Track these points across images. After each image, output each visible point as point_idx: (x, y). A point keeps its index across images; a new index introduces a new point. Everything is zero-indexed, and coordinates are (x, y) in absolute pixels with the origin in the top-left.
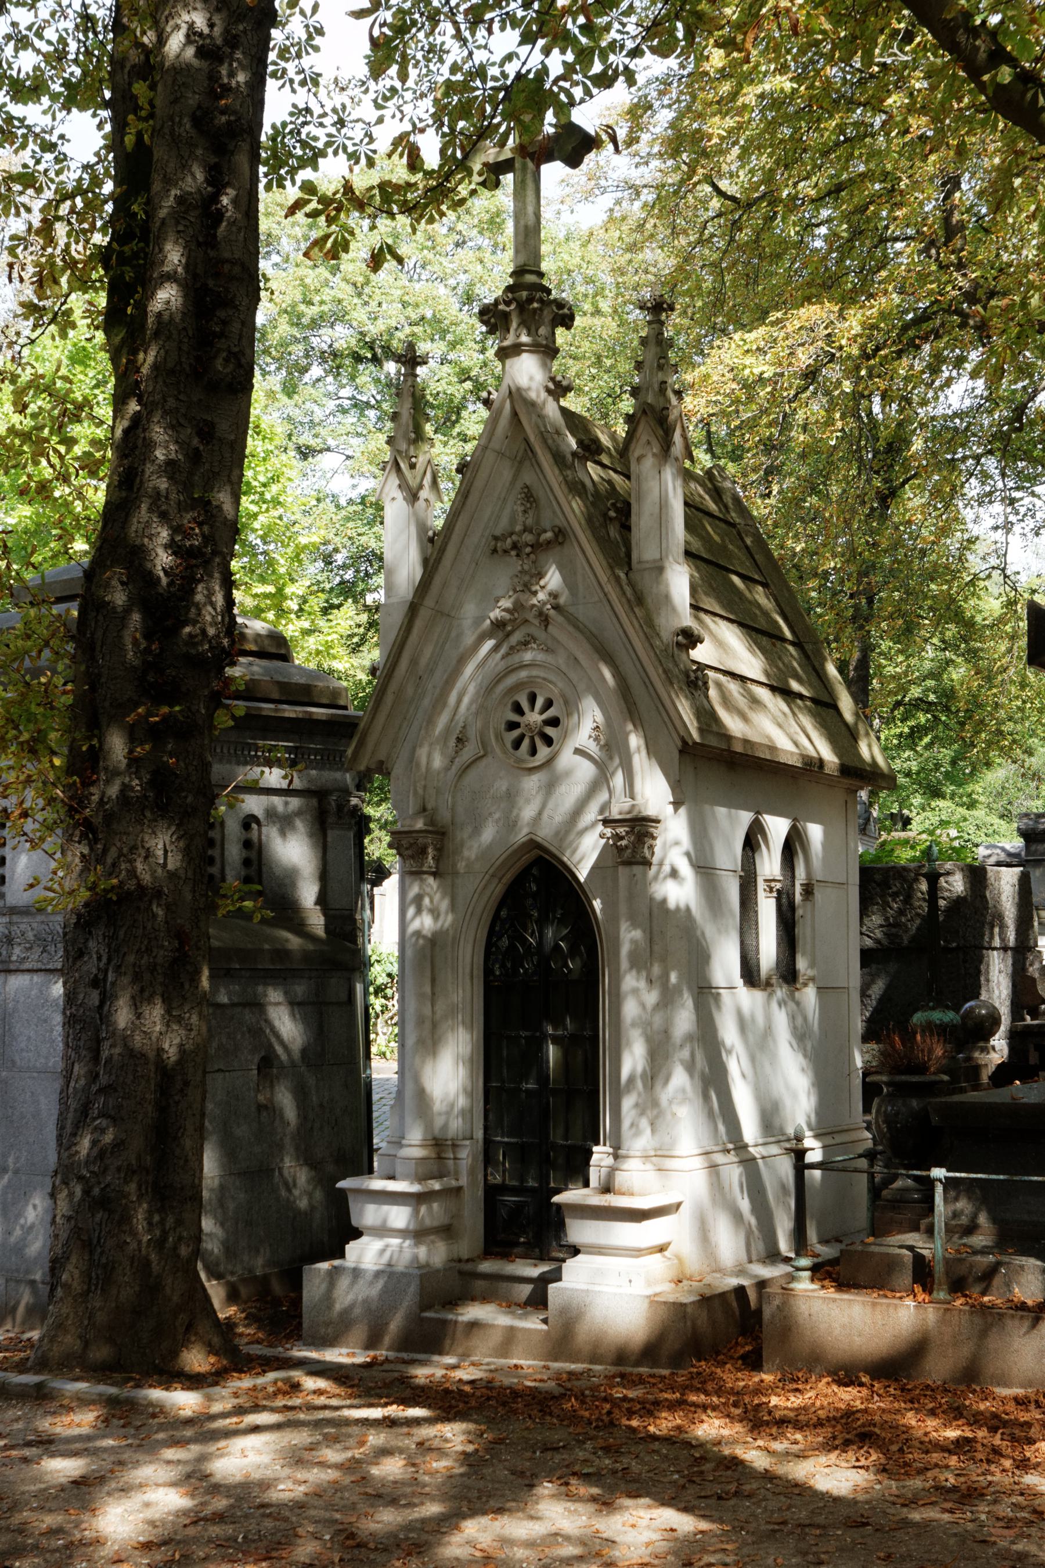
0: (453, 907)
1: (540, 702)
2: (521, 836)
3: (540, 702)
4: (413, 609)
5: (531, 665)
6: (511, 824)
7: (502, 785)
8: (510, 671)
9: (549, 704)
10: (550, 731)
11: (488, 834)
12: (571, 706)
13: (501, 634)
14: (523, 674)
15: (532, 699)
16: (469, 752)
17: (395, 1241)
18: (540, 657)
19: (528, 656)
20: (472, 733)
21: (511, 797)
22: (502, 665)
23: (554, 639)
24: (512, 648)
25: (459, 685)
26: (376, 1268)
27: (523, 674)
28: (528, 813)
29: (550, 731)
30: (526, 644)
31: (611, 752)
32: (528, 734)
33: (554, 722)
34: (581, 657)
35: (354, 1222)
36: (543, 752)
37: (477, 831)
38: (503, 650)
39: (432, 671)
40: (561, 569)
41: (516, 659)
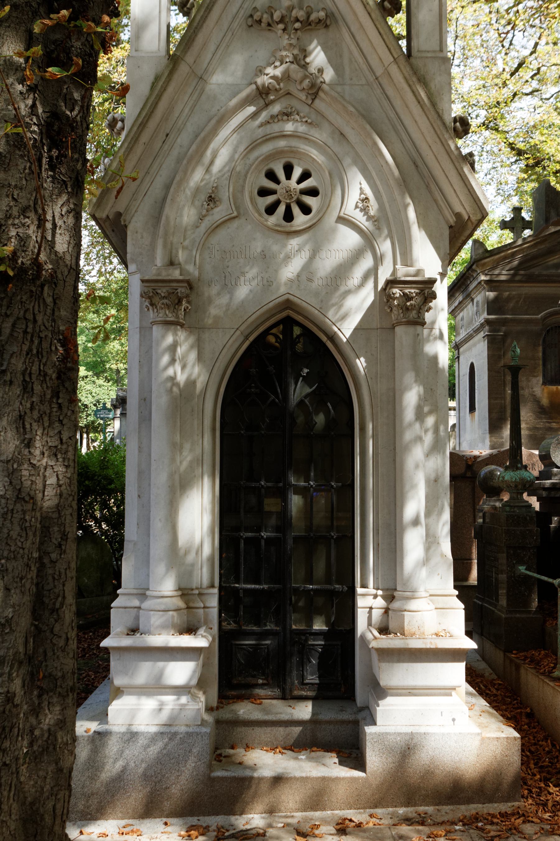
0: (200, 358)
1: (297, 172)
2: (281, 291)
3: (297, 172)
4: (174, 60)
5: (294, 136)
6: (268, 284)
7: (257, 246)
8: (268, 139)
9: (305, 176)
10: (309, 200)
11: (243, 292)
12: (338, 178)
13: (262, 103)
14: (282, 144)
15: (288, 170)
16: (220, 212)
17: (169, 699)
18: (302, 128)
19: (289, 127)
20: (225, 195)
21: (267, 260)
22: (261, 132)
23: (318, 112)
24: (272, 117)
25: (213, 145)
26: (153, 729)
27: (282, 144)
28: (291, 270)
29: (309, 200)
30: (288, 115)
31: (386, 223)
32: (286, 198)
33: (313, 192)
34: (348, 131)
35: (382, 683)
36: (300, 219)
37: (228, 286)
38: (264, 116)
39: (180, 131)
40: (325, 50)
41: (276, 128)
